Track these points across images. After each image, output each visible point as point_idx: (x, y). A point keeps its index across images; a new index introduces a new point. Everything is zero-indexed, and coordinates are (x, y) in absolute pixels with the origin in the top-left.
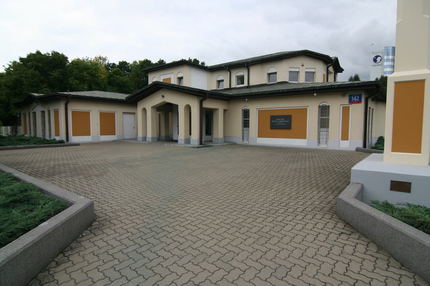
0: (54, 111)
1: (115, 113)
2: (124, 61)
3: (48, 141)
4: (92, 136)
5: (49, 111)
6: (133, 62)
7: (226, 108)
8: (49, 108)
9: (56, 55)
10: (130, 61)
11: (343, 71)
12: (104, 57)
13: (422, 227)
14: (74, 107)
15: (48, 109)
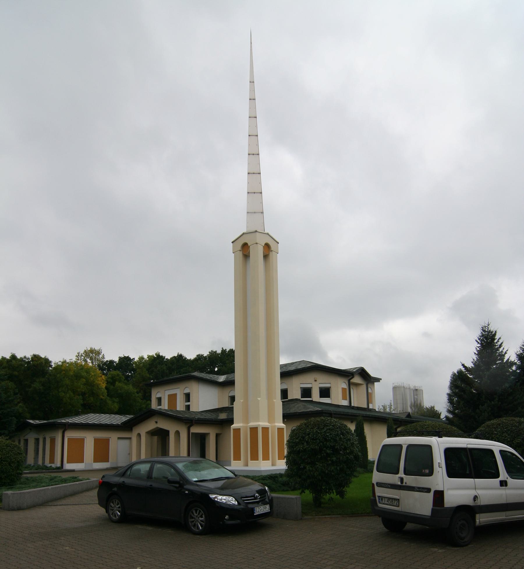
0: (50, 438)
1: (110, 438)
2: (126, 356)
3: (47, 467)
4: (85, 463)
5: (45, 439)
6: (138, 358)
7: (218, 432)
8: (44, 435)
9: (36, 358)
10: (135, 356)
11: (380, 381)
12: (97, 348)
13: (195, 465)
14: (70, 434)
15: (43, 436)
